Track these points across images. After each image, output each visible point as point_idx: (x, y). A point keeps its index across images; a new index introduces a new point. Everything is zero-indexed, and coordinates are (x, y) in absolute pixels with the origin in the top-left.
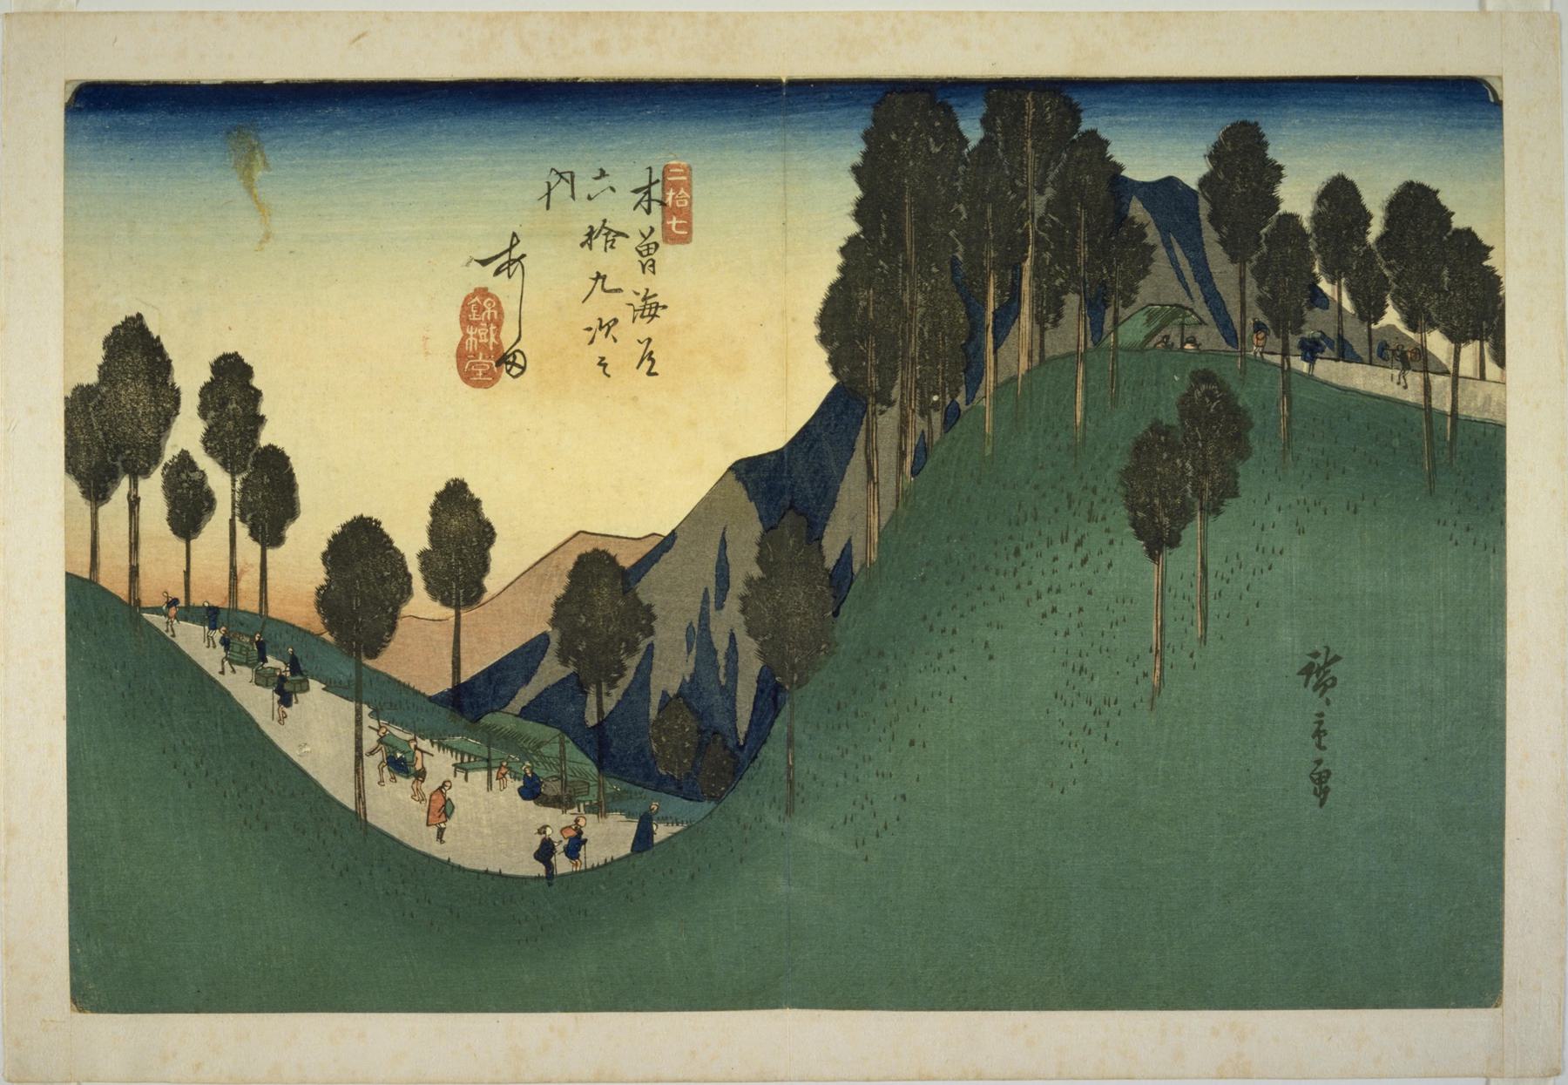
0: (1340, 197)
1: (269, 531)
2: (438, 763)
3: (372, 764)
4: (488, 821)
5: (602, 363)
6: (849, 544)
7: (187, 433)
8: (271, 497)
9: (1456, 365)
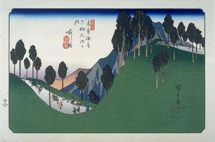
0: (181, 24)
1: (38, 69)
2: (60, 99)
3: (51, 99)
4: (67, 106)
5: (82, 46)
6: (98, 69)
7: (27, 55)
8: (38, 64)
9: (197, 47)
